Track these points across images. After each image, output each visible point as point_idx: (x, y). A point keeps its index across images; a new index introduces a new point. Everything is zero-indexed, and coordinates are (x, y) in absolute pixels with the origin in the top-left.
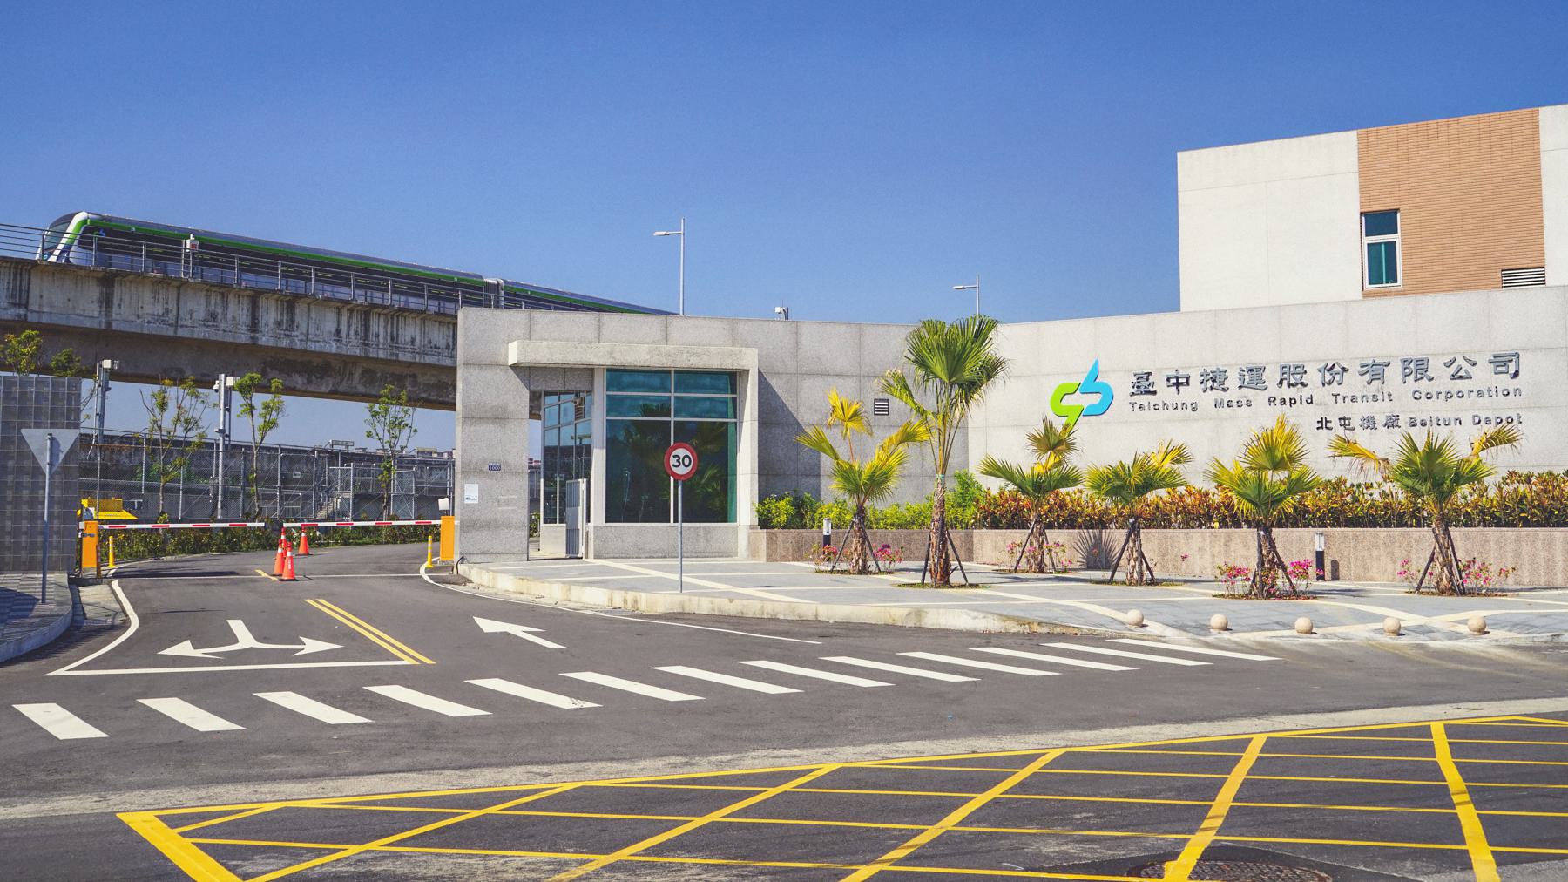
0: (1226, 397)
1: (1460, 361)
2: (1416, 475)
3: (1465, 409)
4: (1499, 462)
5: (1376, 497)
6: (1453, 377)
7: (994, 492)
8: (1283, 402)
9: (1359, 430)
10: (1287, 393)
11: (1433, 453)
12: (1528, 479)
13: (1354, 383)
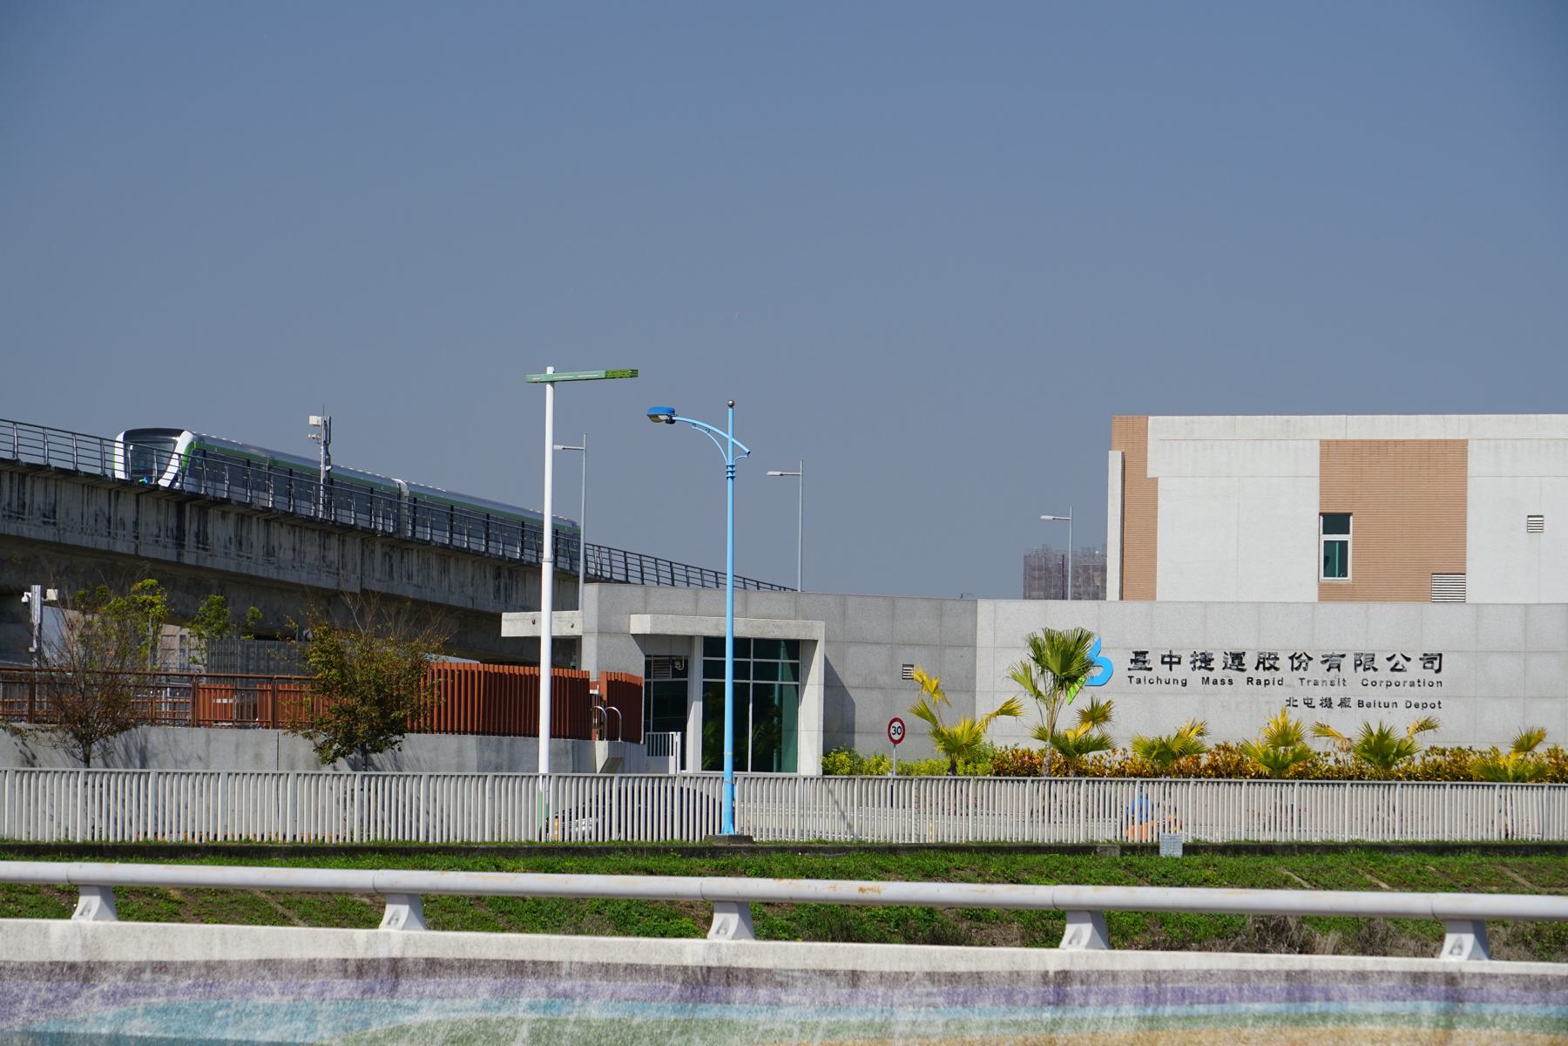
0: (1212, 675)
1: (1399, 658)
2: (1370, 751)
3: (1401, 695)
4: (1424, 742)
5: (1331, 762)
6: (1393, 669)
7: (605, 743)
8: (1259, 682)
9: (1318, 707)
10: (1262, 675)
11: (1383, 736)
12: (1443, 753)
13: (1317, 670)
